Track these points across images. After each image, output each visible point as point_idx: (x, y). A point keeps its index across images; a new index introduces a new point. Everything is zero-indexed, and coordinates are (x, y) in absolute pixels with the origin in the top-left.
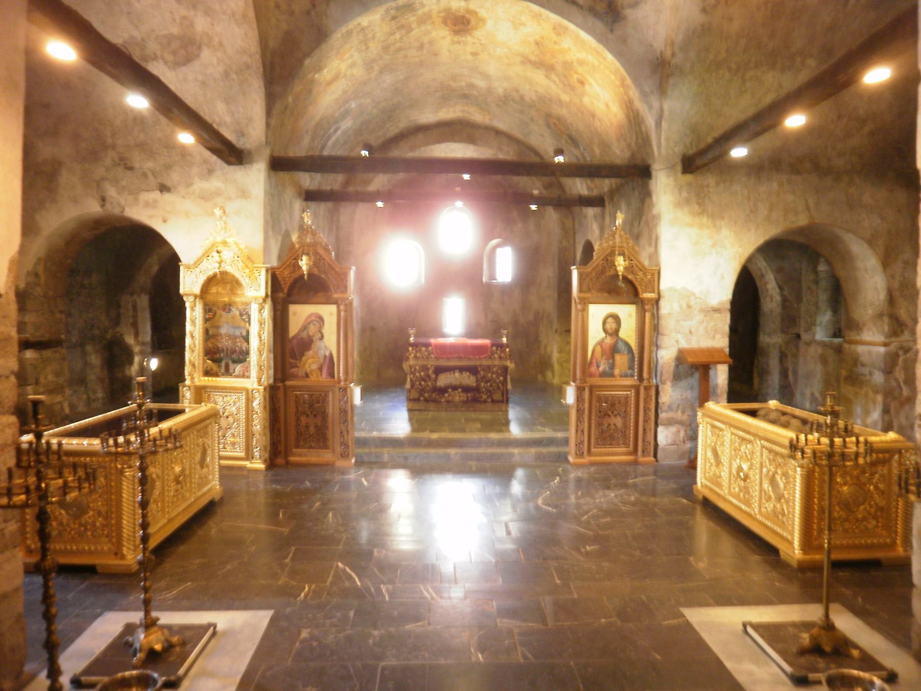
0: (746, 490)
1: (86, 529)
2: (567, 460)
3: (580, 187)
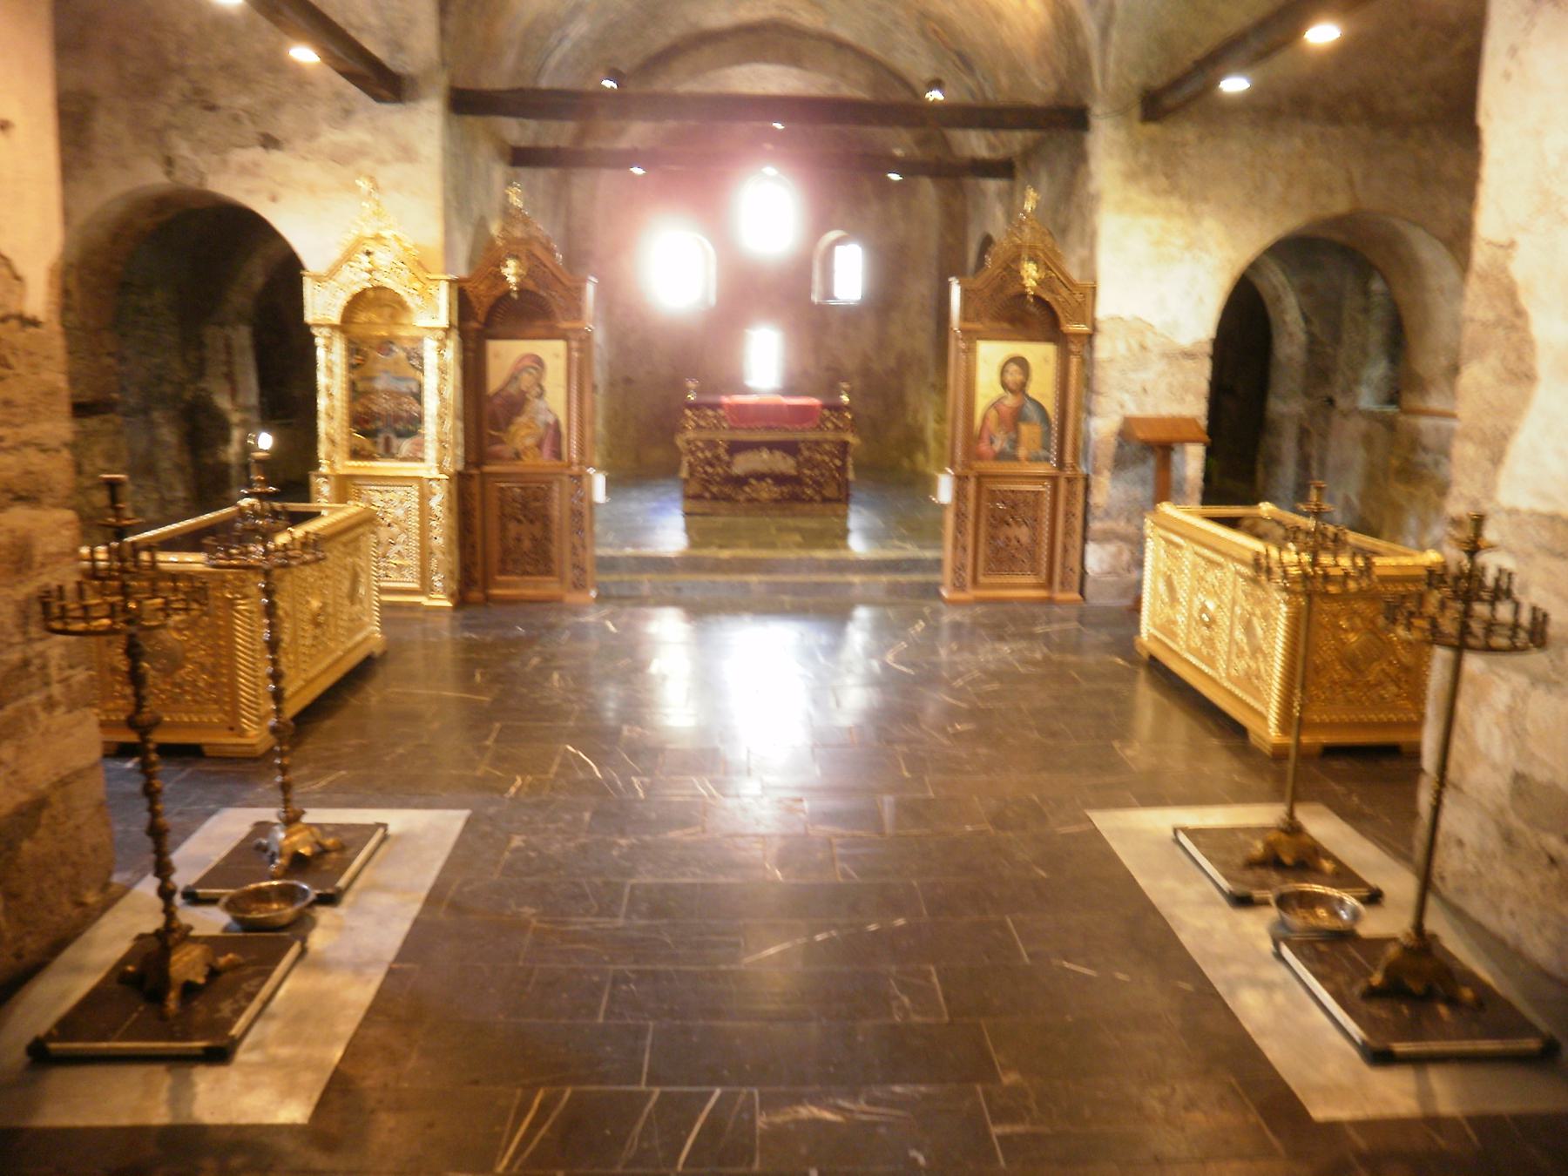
0: (1210, 642)
3: (976, 144)
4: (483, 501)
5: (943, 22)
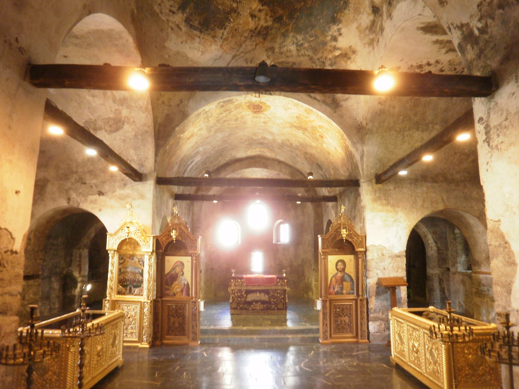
0: (418, 358)
1: (46, 383)
2: (319, 341)
3: (325, 191)
4: (162, 310)
5: (311, 155)
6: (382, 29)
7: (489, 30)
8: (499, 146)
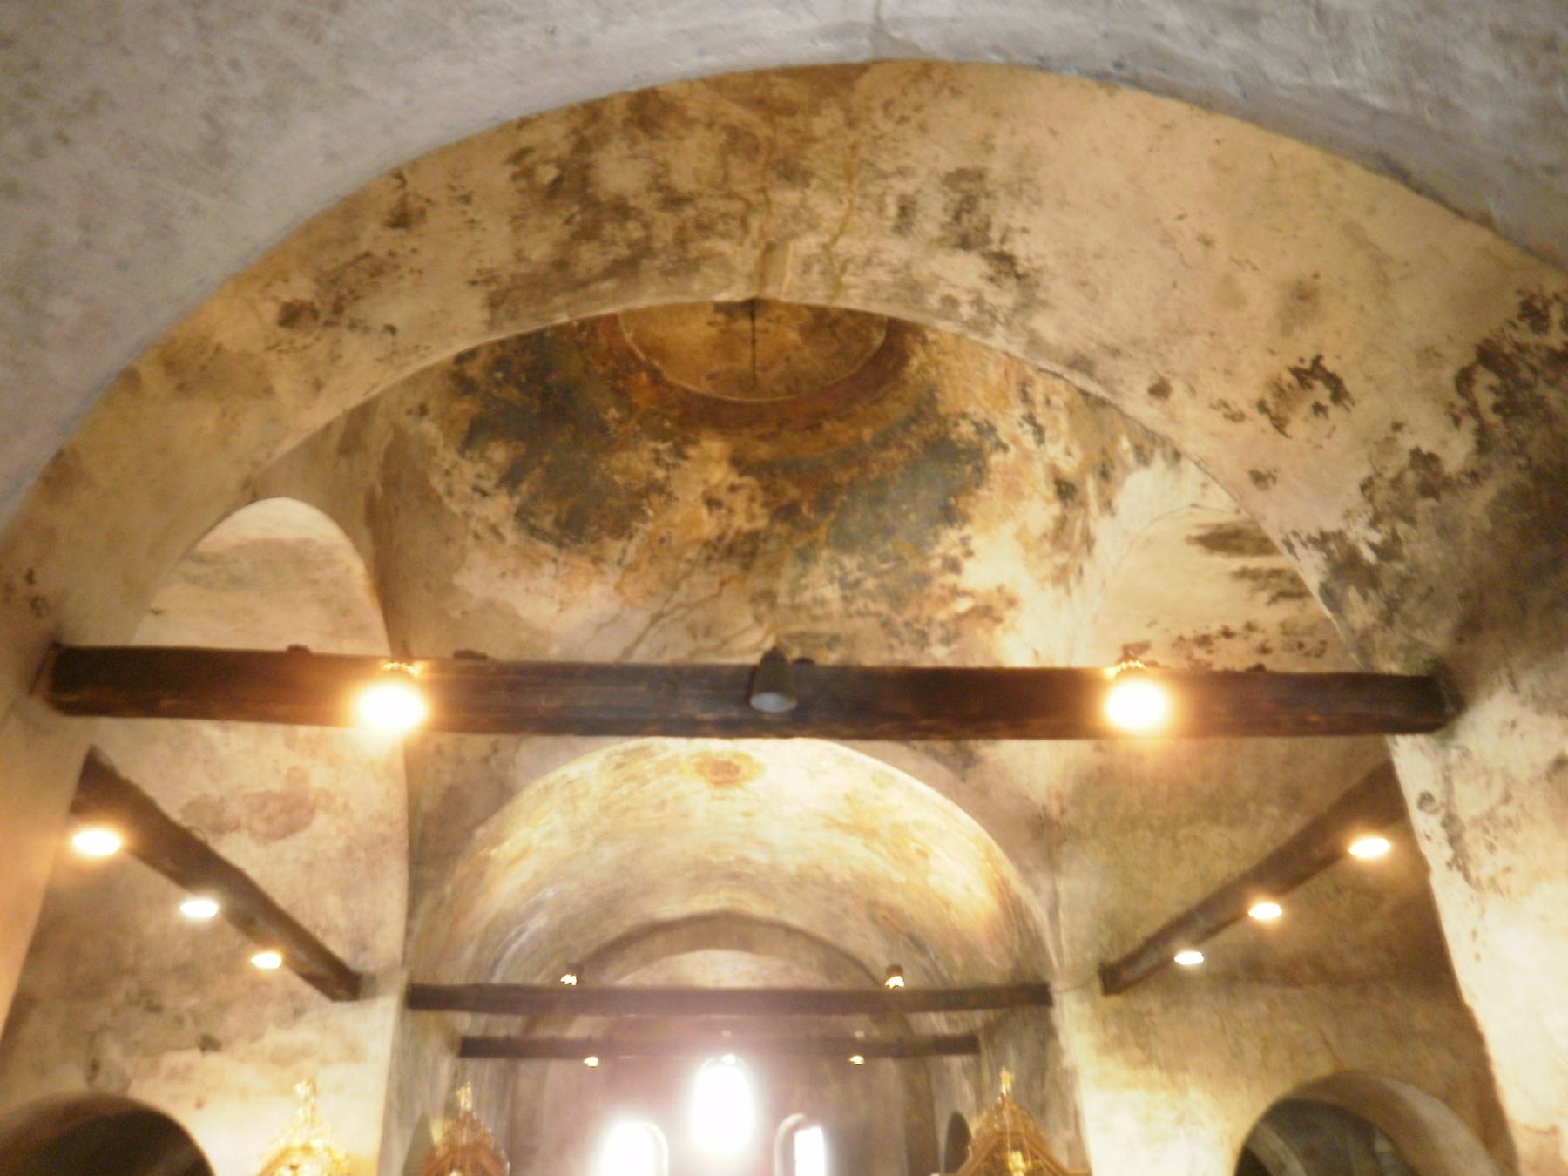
3: (938, 1023)
5: (890, 909)
6: (1089, 541)
7: (1405, 550)
8: (1501, 881)
